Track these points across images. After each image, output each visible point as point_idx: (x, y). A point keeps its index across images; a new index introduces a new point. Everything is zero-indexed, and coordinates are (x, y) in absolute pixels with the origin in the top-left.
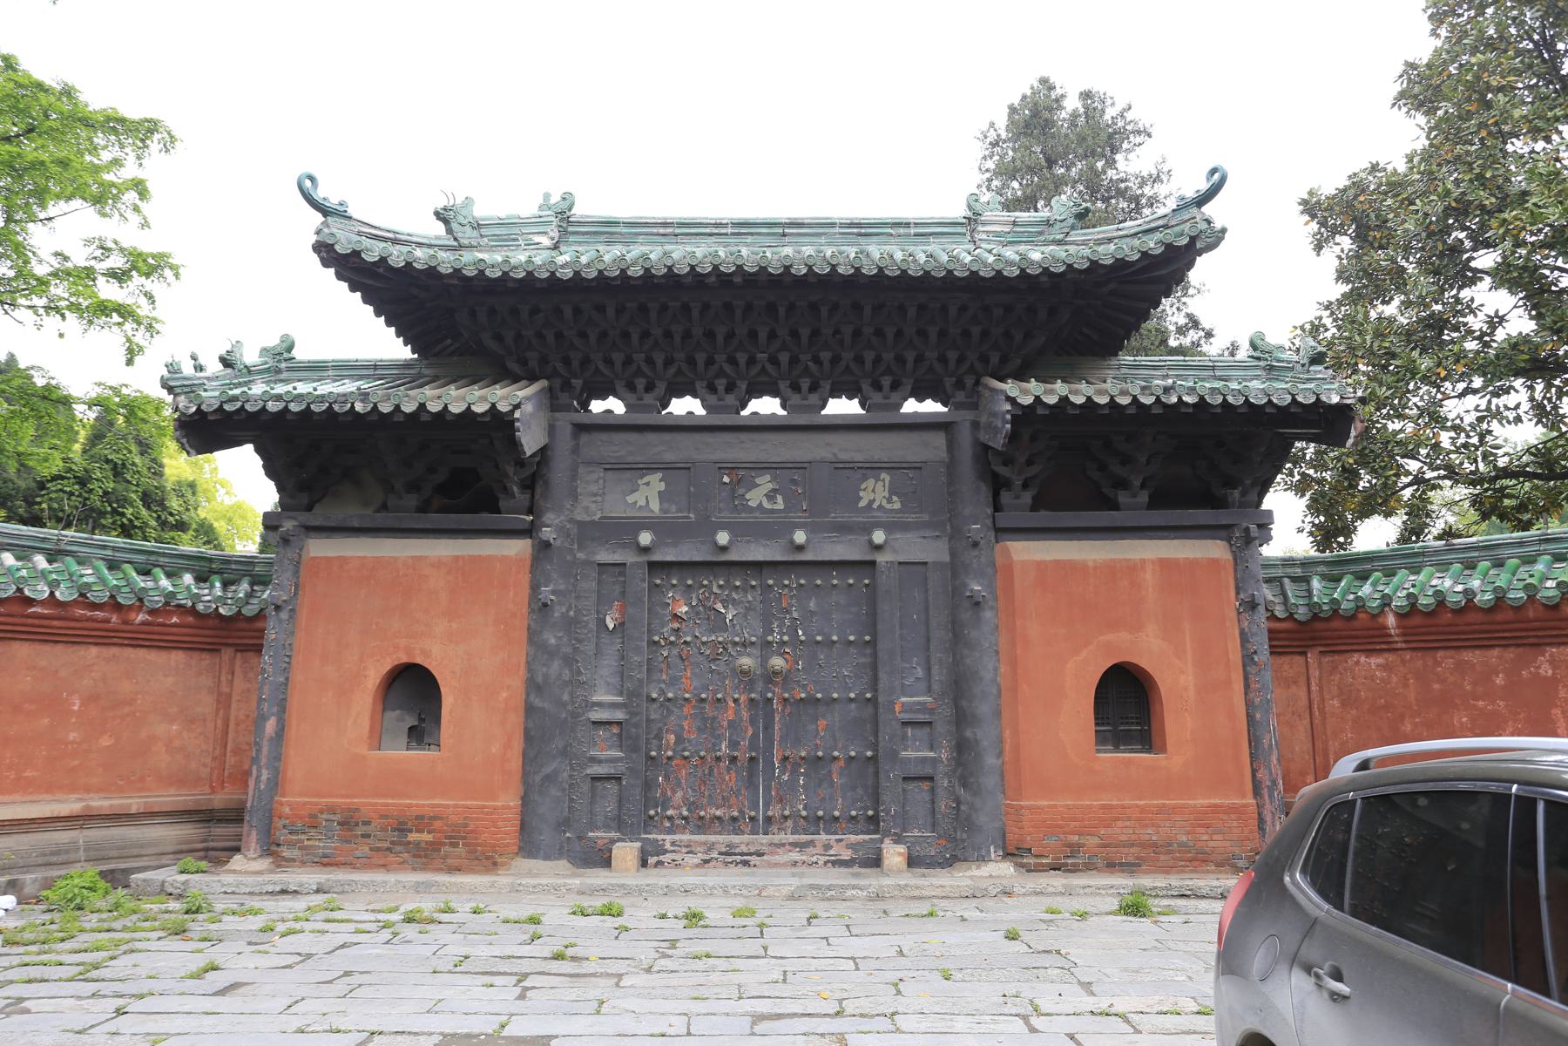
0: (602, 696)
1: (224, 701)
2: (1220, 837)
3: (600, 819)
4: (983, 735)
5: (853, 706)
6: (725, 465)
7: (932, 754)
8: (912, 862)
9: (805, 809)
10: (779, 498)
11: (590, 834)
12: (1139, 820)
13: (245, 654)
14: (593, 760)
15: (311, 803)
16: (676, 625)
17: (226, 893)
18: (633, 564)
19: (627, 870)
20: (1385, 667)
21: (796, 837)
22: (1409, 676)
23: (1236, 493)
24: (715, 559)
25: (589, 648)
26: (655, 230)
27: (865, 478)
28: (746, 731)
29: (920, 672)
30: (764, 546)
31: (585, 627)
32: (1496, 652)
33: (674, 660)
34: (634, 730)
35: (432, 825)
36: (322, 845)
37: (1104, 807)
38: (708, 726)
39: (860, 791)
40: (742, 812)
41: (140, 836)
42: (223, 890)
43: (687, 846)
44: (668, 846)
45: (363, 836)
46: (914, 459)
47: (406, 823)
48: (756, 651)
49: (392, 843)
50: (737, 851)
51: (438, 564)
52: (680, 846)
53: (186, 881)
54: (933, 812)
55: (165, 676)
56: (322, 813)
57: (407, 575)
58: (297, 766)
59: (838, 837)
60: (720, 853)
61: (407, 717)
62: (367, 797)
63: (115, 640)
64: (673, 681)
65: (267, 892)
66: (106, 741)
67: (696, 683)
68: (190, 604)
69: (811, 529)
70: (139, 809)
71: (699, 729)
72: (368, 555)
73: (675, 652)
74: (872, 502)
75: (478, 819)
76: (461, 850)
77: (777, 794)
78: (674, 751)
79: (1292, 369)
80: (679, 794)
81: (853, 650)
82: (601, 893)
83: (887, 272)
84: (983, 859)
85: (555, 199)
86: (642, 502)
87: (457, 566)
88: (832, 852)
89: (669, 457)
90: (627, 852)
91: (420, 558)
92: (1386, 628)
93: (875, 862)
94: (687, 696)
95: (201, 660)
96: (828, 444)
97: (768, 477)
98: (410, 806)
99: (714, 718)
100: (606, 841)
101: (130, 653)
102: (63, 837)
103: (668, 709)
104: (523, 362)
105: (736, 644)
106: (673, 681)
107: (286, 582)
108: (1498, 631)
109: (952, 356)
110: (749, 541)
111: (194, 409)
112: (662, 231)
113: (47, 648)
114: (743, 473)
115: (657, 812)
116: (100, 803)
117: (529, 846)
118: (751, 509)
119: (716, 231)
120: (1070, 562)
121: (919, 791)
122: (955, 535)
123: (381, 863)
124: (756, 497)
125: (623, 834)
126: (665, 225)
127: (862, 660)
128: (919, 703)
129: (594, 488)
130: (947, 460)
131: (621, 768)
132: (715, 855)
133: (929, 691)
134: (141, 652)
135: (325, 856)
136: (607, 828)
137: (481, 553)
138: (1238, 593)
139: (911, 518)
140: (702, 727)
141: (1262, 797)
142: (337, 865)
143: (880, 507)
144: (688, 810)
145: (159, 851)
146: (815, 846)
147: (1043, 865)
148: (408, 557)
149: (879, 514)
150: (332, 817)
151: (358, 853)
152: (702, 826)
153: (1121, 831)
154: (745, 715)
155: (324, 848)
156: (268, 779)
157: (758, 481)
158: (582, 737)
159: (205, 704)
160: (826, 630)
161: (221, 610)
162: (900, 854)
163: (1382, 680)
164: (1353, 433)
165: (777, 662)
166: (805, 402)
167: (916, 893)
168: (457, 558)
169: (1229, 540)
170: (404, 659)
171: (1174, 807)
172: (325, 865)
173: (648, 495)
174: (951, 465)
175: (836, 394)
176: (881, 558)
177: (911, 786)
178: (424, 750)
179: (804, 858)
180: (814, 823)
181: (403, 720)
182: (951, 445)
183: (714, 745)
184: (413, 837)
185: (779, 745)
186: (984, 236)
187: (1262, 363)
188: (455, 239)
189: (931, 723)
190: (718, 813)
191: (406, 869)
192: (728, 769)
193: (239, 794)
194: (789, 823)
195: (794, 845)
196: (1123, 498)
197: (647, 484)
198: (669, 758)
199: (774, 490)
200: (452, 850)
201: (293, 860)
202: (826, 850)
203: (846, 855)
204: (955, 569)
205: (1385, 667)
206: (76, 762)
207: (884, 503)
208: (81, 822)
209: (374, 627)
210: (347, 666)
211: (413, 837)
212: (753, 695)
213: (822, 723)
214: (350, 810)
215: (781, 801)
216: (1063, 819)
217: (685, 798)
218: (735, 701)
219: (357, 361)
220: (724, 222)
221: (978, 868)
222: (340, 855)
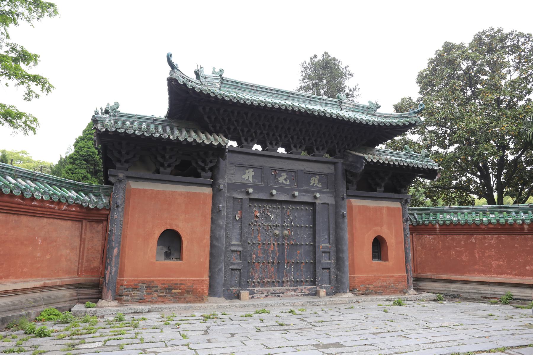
0: (234, 242)
1: (82, 241)
2: (400, 284)
3: (233, 283)
4: (347, 256)
5: (307, 247)
6: (273, 169)
7: (330, 261)
8: (328, 294)
9: (293, 278)
10: (288, 181)
11: (231, 288)
12: (382, 280)
13: (91, 223)
14: (232, 263)
15: (134, 280)
16: (256, 219)
17: (113, 314)
18: (245, 199)
19: (246, 300)
20: (434, 239)
21: (292, 288)
22: (440, 241)
23: (403, 190)
24: (270, 199)
25: (231, 226)
26: (251, 88)
27: (312, 177)
28: (277, 254)
29: (326, 237)
30: (284, 195)
31: (229, 219)
32: (462, 236)
33: (255, 231)
34: (245, 254)
35: (180, 286)
36: (139, 295)
37: (374, 276)
38: (266, 252)
39: (309, 273)
40: (275, 280)
41: (58, 294)
42: (111, 313)
44: (255, 292)
45: (155, 291)
46: (326, 172)
47: (171, 286)
48: (279, 229)
49: (166, 293)
50: (276, 292)
51: (181, 194)
52: (259, 291)
53: (95, 310)
54: (330, 278)
55: (66, 231)
56: (139, 283)
57: (169, 197)
58: (128, 268)
59: (305, 287)
60: (271, 293)
61: (164, 248)
62: (156, 277)
63: (53, 216)
64: (255, 237)
65: (129, 313)
66: (48, 257)
67: (262, 238)
68: (81, 203)
69: (299, 191)
70: (59, 284)
71: (263, 253)
72: (162, 190)
73: (256, 228)
74: (314, 184)
75: (197, 284)
76: (191, 295)
78: (255, 260)
79: (418, 157)
80: (257, 275)
81: (307, 229)
82: (247, 307)
83: (339, 118)
84: (345, 292)
85: (217, 70)
86: (247, 178)
87: (188, 195)
88: (303, 292)
89: (256, 164)
90: (245, 294)
91: (174, 192)
92: (436, 228)
93: (316, 294)
94: (260, 242)
95: (76, 225)
96: (302, 165)
97: (285, 174)
98: (172, 280)
99: (267, 250)
100: (236, 290)
101: (56, 221)
102: (36, 295)
103: (253, 247)
104: (214, 127)
105: (274, 226)
106: (255, 237)
107: (121, 197)
108: (464, 231)
109: (246, 130)
110: (280, 194)
111: (104, 130)
112: (253, 88)
113: (31, 219)
114: (278, 171)
115: (250, 280)
116: (49, 282)
117: (212, 292)
118: (280, 184)
119: (270, 91)
120: (366, 206)
121: (326, 272)
122: (336, 197)
123: (162, 301)
124: (281, 180)
125: (242, 288)
126: (254, 86)
127: (310, 232)
128: (326, 246)
129: (232, 172)
130: (334, 173)
131: (241, 266)
132: (270, 294)
133: (329, 243)
134: (59, 221)
135: (141, 299)
136: (236, 286)
137: (380, 205)
138: (403, 217)
139: (325, 190)
141: (408, 273)
142: (145, 302)
143: (316, 186)
144: (260, 280)
145: (65, 300)
147: (360, 293)
148: (170, 191)
149: (316, 188)
150: (143, 285)
151: (153, 298)
152: (264, 284)
153: (378, 283)
154: (276, 249)
155: (140, 296)
156: (115, 271)
157: (282, 174)
158: (229, 256)
159: (77, 243)
160: (300, 223)
161: (90, 206)
162: (324, 291)
163: (433, 242)
164: (437, 177)
165: (286, 232)
166: (297, 151)
167: (335, 302)
168: (188, 192)
169: (401, 202)
170: (169, 228)
171: (391, 276)
172: (140, 302)
173: (249, 176)
174: (336, 174)
175: (258, 144)
176: (317, 202)
177: (324, 271)
178: (171, 260)
179: (295, 294)
180: (297, 283)
181: (162, 249)
182: (335, 169)
183: (267, 258)
184: (173, 291)
185: (286, 258)
186: (344, 107)
187: (408, 154)
188: (200, 82)
190: (269, 280)
191: (171, 302)
192: (272, 266)
193: (90, 277)
194: (289, 283)
195: (293, 290)
196: (203, 174)
197: (249, 172)
198: (254, 263)
199: (287, 178)
200: (187, 295)
201: (128, 301)
202: (301, 291)
203: (307, 292)
204: (337, 206)
205: (434, 239)
206: (39, 265)
207: (317, 184)
208: (41, 289)
209: (157, 215)
210: (147, 229)
211: (173, 291)
212: (278, 243)
213: (298, 252)
214: (150, 282)
215: (287, 276)
217: (258, 276)
218: (274, 244)
219: (146, 116)
220: (272, 89)
221: (344, 295)
222: (147, 299)
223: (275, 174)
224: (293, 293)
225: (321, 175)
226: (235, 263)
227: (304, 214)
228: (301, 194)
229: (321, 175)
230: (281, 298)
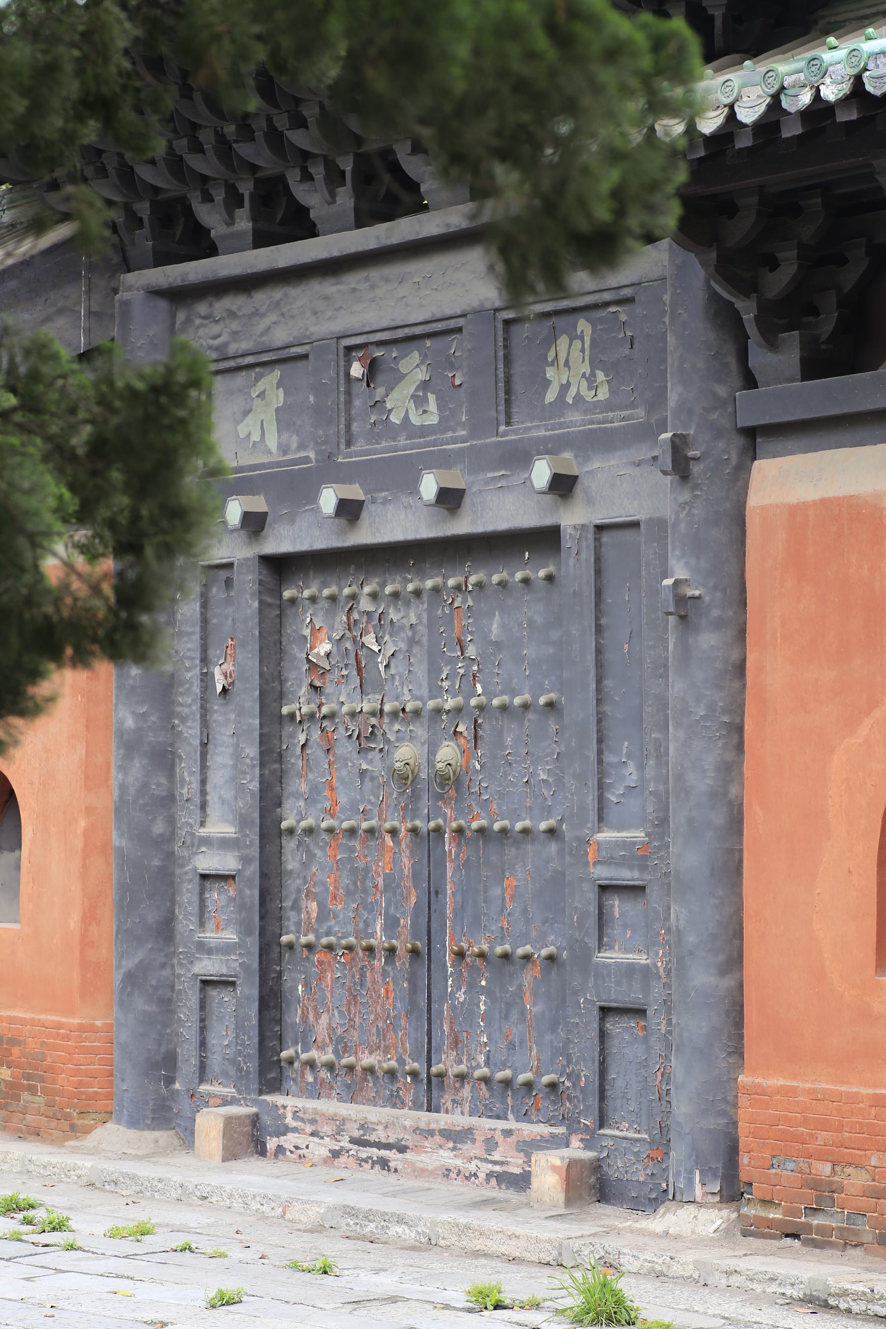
28: (407, 899)
40: (401, 1061)
43: (313, 1122)
44: (289, 1120)
48: (420, 730)
52: (302, 1120)
60: (353, 1141)
74: (565, 388)
77: (451, 1029)
80: (324, 1020)
88: (496, 1156)
132: (346, 1144)
140: (352, 887)
143: (578, 398)
146: (474, 1141)
147: (770, 1223)
162: (554, 1168)
167: (479, 1244)
179: (459, 1162)
189: (642, 889)
216: (805, 1122)
223: (373, 368)
224: (446, 1157)
225: (607, 304)
226: (213, 943)
227: (539, 619)
228: (488, 482)
229: (607, 304)
230: (392, 1178)
